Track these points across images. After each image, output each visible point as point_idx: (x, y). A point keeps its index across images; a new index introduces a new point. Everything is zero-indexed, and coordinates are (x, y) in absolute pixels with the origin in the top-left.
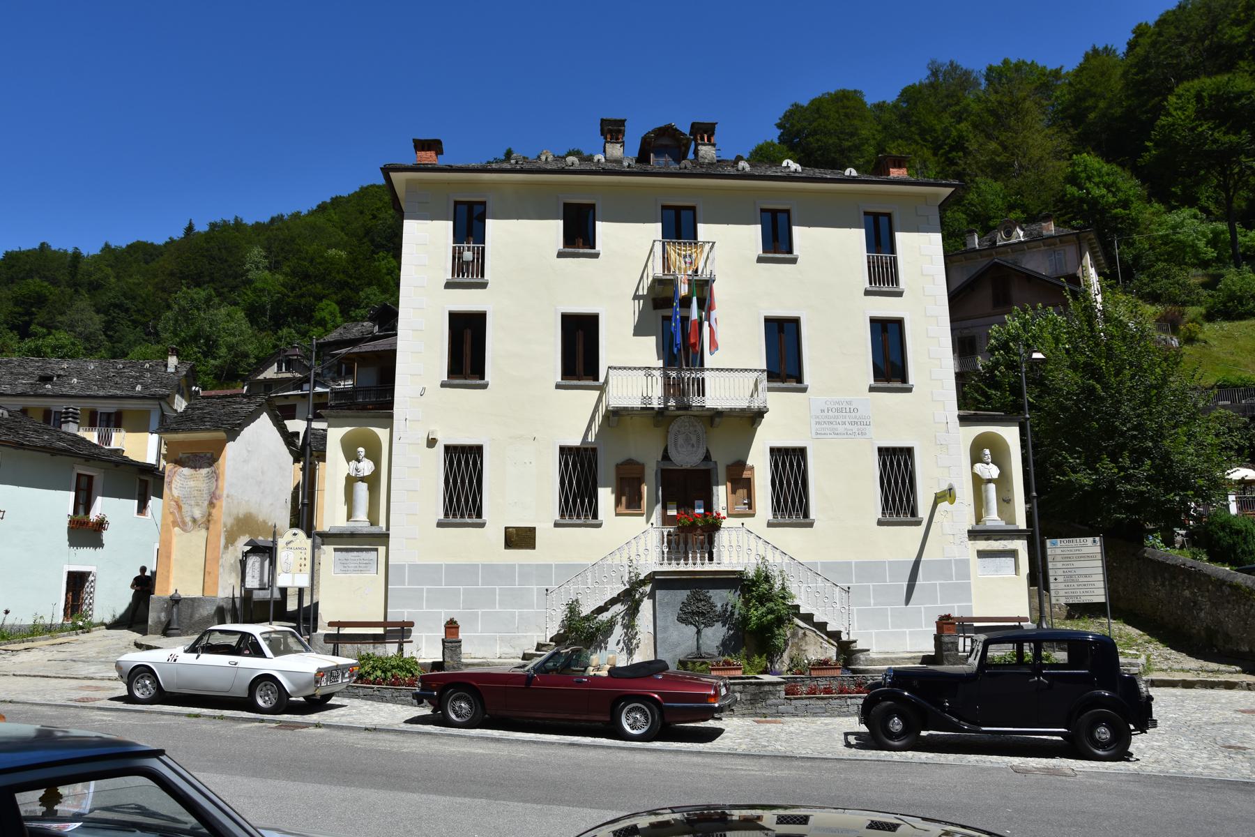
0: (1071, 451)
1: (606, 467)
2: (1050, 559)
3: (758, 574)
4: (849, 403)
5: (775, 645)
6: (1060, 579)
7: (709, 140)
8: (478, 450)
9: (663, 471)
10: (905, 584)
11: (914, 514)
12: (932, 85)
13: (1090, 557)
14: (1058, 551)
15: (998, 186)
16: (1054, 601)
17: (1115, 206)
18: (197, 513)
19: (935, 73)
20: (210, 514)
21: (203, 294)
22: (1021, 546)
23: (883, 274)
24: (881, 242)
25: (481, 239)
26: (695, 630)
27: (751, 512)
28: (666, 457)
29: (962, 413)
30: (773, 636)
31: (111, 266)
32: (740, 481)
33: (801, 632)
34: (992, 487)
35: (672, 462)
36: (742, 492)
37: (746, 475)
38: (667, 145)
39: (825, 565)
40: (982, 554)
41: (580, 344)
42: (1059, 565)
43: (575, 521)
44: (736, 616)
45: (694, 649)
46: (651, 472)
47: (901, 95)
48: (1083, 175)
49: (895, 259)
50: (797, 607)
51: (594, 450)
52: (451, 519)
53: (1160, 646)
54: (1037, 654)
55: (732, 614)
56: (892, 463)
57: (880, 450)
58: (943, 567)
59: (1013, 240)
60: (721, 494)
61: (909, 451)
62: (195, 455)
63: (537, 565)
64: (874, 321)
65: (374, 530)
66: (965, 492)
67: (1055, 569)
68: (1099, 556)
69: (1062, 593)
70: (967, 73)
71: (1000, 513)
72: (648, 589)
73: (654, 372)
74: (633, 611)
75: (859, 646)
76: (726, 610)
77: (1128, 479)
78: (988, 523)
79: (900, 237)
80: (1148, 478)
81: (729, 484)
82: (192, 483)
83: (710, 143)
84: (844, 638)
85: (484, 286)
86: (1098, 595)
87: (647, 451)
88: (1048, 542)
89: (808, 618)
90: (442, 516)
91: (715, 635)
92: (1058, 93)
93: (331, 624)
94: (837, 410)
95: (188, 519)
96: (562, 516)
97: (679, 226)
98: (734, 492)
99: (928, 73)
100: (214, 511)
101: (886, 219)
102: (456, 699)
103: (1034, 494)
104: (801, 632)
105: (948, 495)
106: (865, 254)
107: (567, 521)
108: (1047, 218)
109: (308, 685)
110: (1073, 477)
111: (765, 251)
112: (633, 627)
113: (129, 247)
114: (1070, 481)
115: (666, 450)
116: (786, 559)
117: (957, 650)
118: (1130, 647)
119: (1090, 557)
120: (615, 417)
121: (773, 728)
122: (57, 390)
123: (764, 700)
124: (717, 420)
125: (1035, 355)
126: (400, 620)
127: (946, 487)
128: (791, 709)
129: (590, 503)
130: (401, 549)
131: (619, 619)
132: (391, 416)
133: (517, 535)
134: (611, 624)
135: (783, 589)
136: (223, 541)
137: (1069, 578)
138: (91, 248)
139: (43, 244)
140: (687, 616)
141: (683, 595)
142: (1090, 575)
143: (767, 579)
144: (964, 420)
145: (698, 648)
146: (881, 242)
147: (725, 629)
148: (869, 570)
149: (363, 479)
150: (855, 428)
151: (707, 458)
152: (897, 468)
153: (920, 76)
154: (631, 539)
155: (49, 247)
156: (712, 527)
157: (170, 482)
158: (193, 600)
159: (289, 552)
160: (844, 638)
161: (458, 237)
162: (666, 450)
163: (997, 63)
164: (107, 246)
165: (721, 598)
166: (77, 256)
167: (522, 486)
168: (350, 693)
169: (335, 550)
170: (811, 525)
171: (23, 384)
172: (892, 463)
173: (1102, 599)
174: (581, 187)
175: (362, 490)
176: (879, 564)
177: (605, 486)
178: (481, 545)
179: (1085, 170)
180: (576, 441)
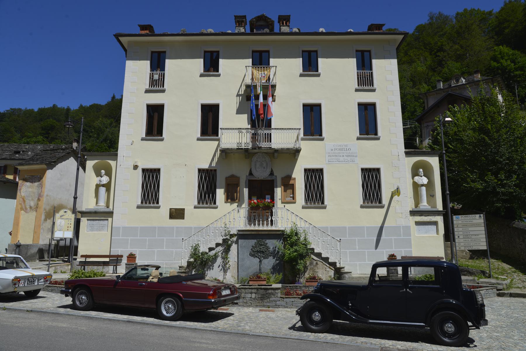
0: (472, 172)
1: (220, 179)
2: (455, 226)
3: (292, 232)
4: (346, 146)
5: (299, 269)
6: (461, 237)
7: (286, 24)
8: (158, 170)
9: (249, 181)
10: (375, 238)
11: (380, 202)
12: (430, 24)
13: (477, 225)
14: (460, 222)
15: (458, 65)
16: (458, 249)
17: (516, 69)
18: (32, 204)
19: (431, 18)
20: (38, 204)
21: (109, 121)
22: (440, 219)
23: (366, 81)
24: (364, 64)
25: (163, 69)
26: (258, 260)
27: (294, 201)
28: (251, 174)
29: (407, 150)
30: (297, 264)
31: (83, 114)
32: (288, 185)
33: (315, 262)
34: (424, 188)
35: (253, 176)
36: (289, 191)
37: (291, 182)
38: (261, 24)
39: (333, 229)
40: (418, 223)
41: (210, 117)
42: (461, 229)
43: (205, 205)
44: (280, 253)
45: (258, 271)
46: (243, 181)
47: (416, 29)
48: (499, 56)
49: (372, 73)
50: (313, 249)
51: (215, 170)
52: (144, 205)
53: (521, 274)
54: (405, 272)
55: (278, 252)
56: (369, 176)
57: (362, 170)
58: (396, 229)
59: (460, 84)
60: (279, 192)
61: (378, 170)
62: (32, 176)
63: (185, 227)
64: (360, 105)
65: (107, 210)
66: (408, 191)
67: (458, 232)
68: (483, 225)
69: (462, 244)
70: (446, 17)
71: (428, 202)
72: (235, 239)
73: (243, 131)
74: (227, 250)
75: (346, 270)
76: (275, 250)
77: (503, 186)
78: (421, 207)
79: (374, 62)
80: (515, 185)
81: (283, 187)
82: (30, 190)
83: (287, 25)
84: (338, 265)
85: (163, 91)
86: (483, 245)
87: (241, 171)
88: (454, 217)
89: (319, 255)
90: (140, 203)
91: (269, 263)
92: (490, 22)
93: (82, 256)
94: (340, 149)
95: (28, 207)
96: (199, 203)
97: (261, 60)
98: (285, 191)
99: (428, 18)
100: (39, 203)
101: (368, 53)
102: (81, 294)
103: (448, 192)
104: (315, 262)
105: (397, 192)
106: (356, 71)
107: (201, 205)
108: (476, 72)
109: (8, 286)
110: (473, 185)
111: (304, 71)
112: (227, 258)
113: (91, 106)
114: (470, 187)
115: (251, 170)
116: (307, 225)
117: (397, 273)
118: (503, 274)
119: (477, 225)
120: (225, 153)
121: (271, 314)
122: (21, 157)
123: (269, 298)
124: (276, 154)
125: (447, 119)
126: (117, 254)
127: (396, 188)
128: (283, 303)
129: (213, 196)
130: (118, 220)
131: (220, 254)
132: (117, 155)
133: (176, 212)
134: (216, 257)
135: (305, 240)
136: (43, 217)
137: (466, 236)
138: (74, 107)
139: (54, 105)
140: (254, 253)
141: (253, 242)
142: (478, 235)
143: (296, 234)
144: (407, 154)
145: (260, 270)
146: (364, 64)
147: (274, 260)
148: (356, 231)
149: (103, 186)
150: (349, 158)
151: (272, 174)
152: (371, 179)
153: (424, 20)
154: (231, 215)
155: (57, 106)
156: (269, 209)
157: (20, 189)
158: (28, 245)
159: (62, 220)
160: (338, 265)
161: (153, 68)
162: (251, 170)
163: (461, 10)
164: (81, 106)
165: (272, 244)
166: (68, 110)
167: (179, 188)
168: (46, 289)
169: (88, 220)
170: (325, 208)
171: (6, 154)
172: (369, 176)
173: (485, 248)
174: (213, 42)
175: (103, 190)
176: (362, 228)
177: (220, 188)
178: (158, 217)
179: (500, 54)
180: (206, 166)
